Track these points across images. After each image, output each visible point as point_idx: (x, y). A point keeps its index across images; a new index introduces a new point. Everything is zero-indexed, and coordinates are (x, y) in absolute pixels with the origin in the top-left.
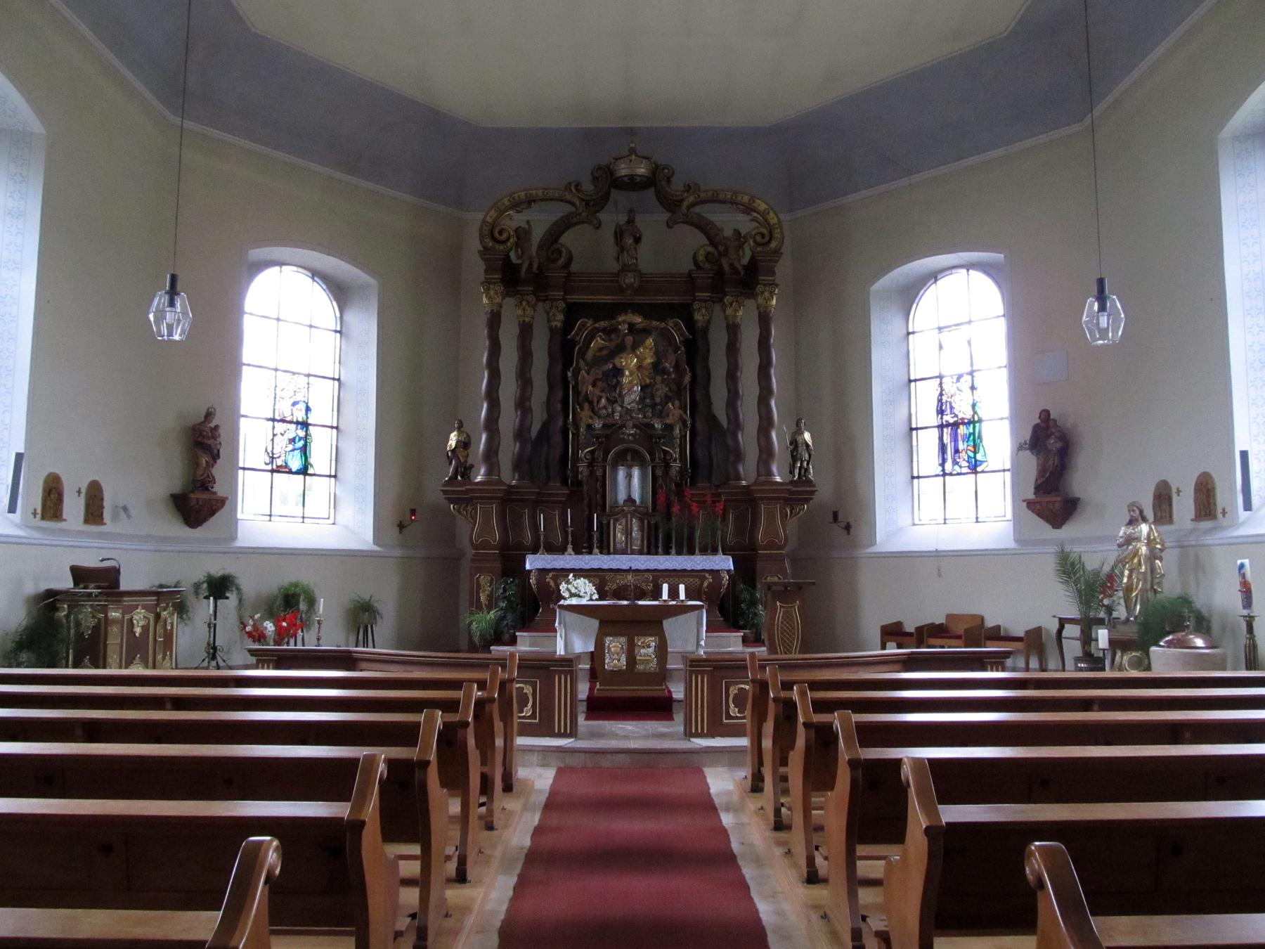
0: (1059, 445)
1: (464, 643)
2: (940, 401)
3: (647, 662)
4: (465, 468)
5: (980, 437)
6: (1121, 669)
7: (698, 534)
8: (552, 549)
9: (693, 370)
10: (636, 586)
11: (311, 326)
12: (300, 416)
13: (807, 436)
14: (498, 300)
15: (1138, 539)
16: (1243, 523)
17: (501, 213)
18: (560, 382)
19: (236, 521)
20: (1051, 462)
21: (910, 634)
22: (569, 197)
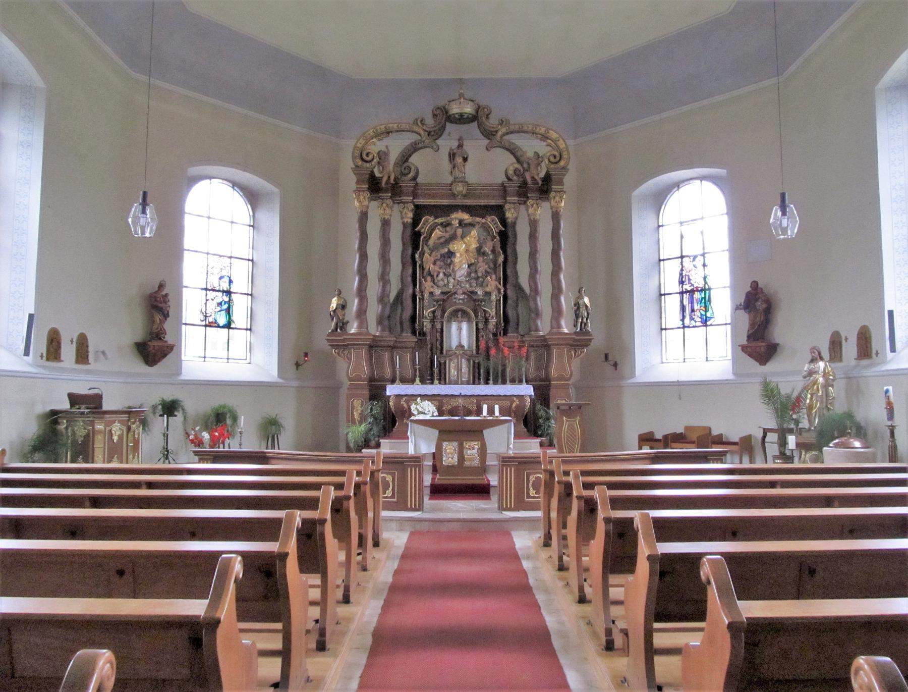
0: (764, 306)
1: (343, 446)
2: (681, 274)
3: (472, 459)
4: (343, 324)
5: (709, 300)
6: (804, 462)
7: (508, 370)
8: (404, 381)
9: (505, 252)
10: (464, 407)
11: (232, 222)
12: (225, 286)
13: (586, 300)
14: (366, 203)
15: (817, 372)
16: (890, 361)
17: (367, 141)
18: (412, 264)
19: (181, 361)
20: (758, 319)
21: (659, 440)
22: (416, 129)
